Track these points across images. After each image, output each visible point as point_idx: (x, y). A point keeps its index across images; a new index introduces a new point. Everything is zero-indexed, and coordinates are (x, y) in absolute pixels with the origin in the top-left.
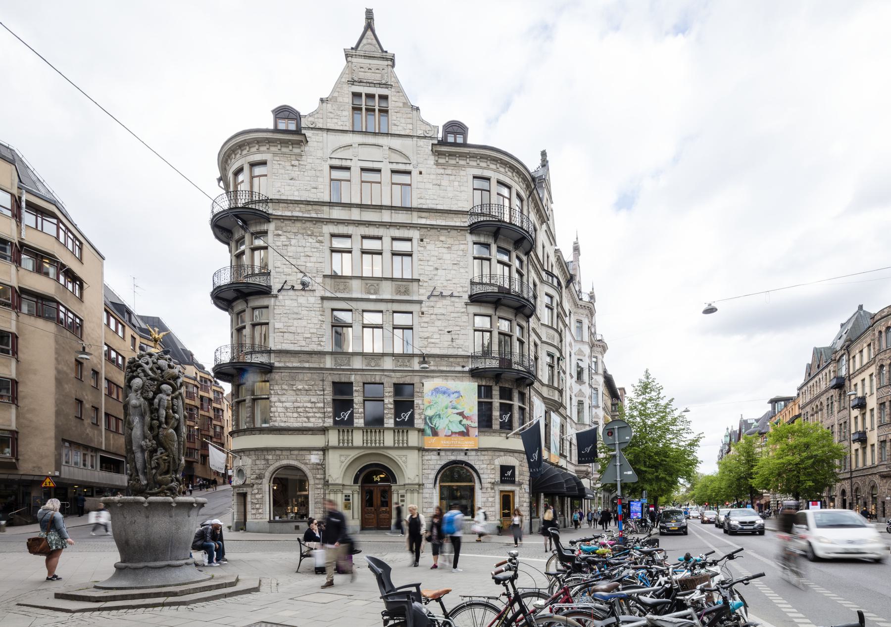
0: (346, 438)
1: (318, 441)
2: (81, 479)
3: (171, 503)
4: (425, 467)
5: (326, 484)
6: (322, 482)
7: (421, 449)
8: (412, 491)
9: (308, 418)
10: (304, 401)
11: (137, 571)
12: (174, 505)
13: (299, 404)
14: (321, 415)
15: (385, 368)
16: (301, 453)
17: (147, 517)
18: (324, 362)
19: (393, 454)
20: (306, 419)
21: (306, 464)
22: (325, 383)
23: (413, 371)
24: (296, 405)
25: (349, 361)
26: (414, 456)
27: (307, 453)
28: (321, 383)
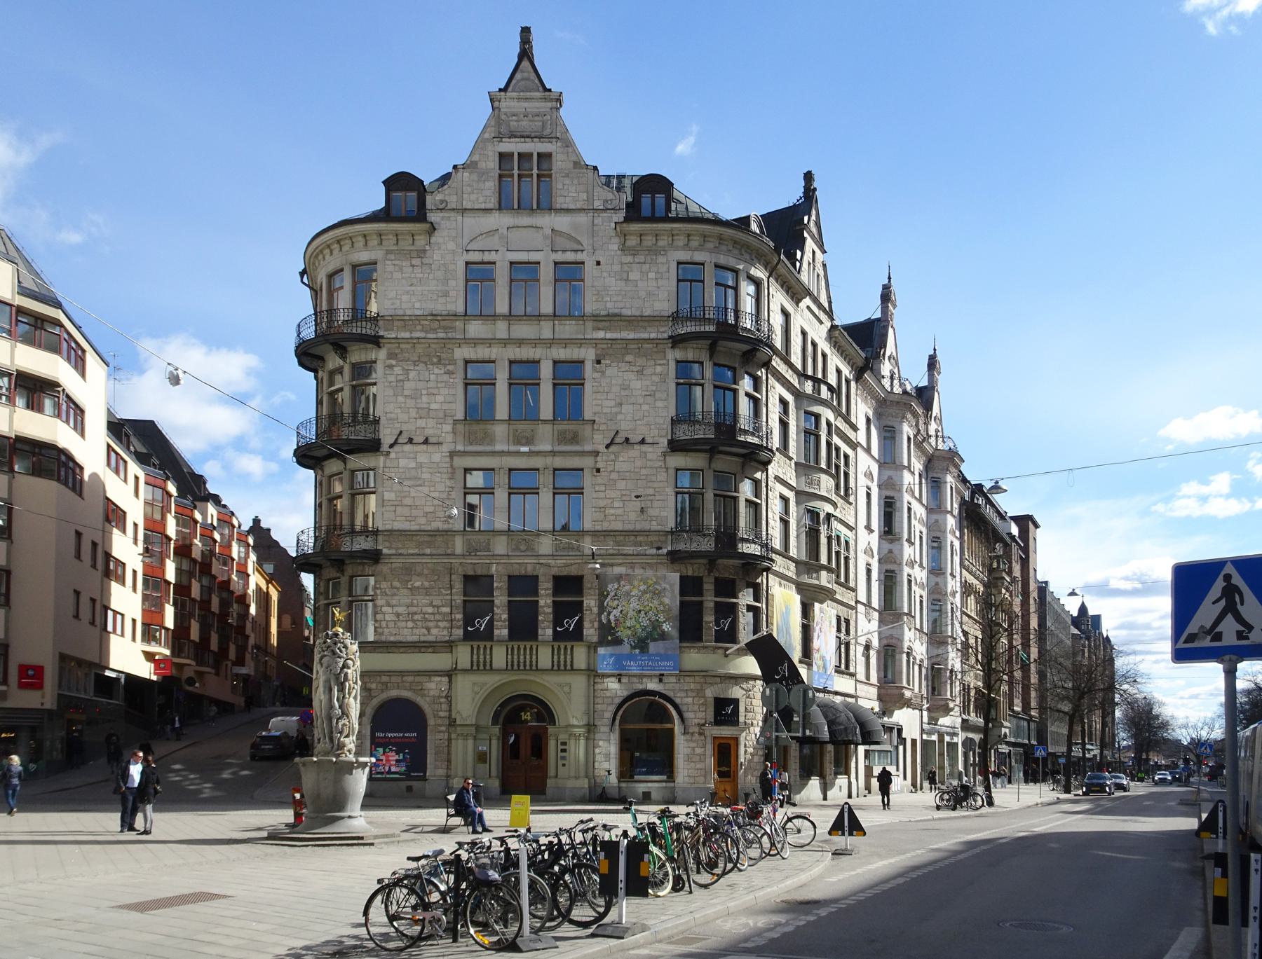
1: (441, 661)
9: (428, 629)
13: (415, 609)
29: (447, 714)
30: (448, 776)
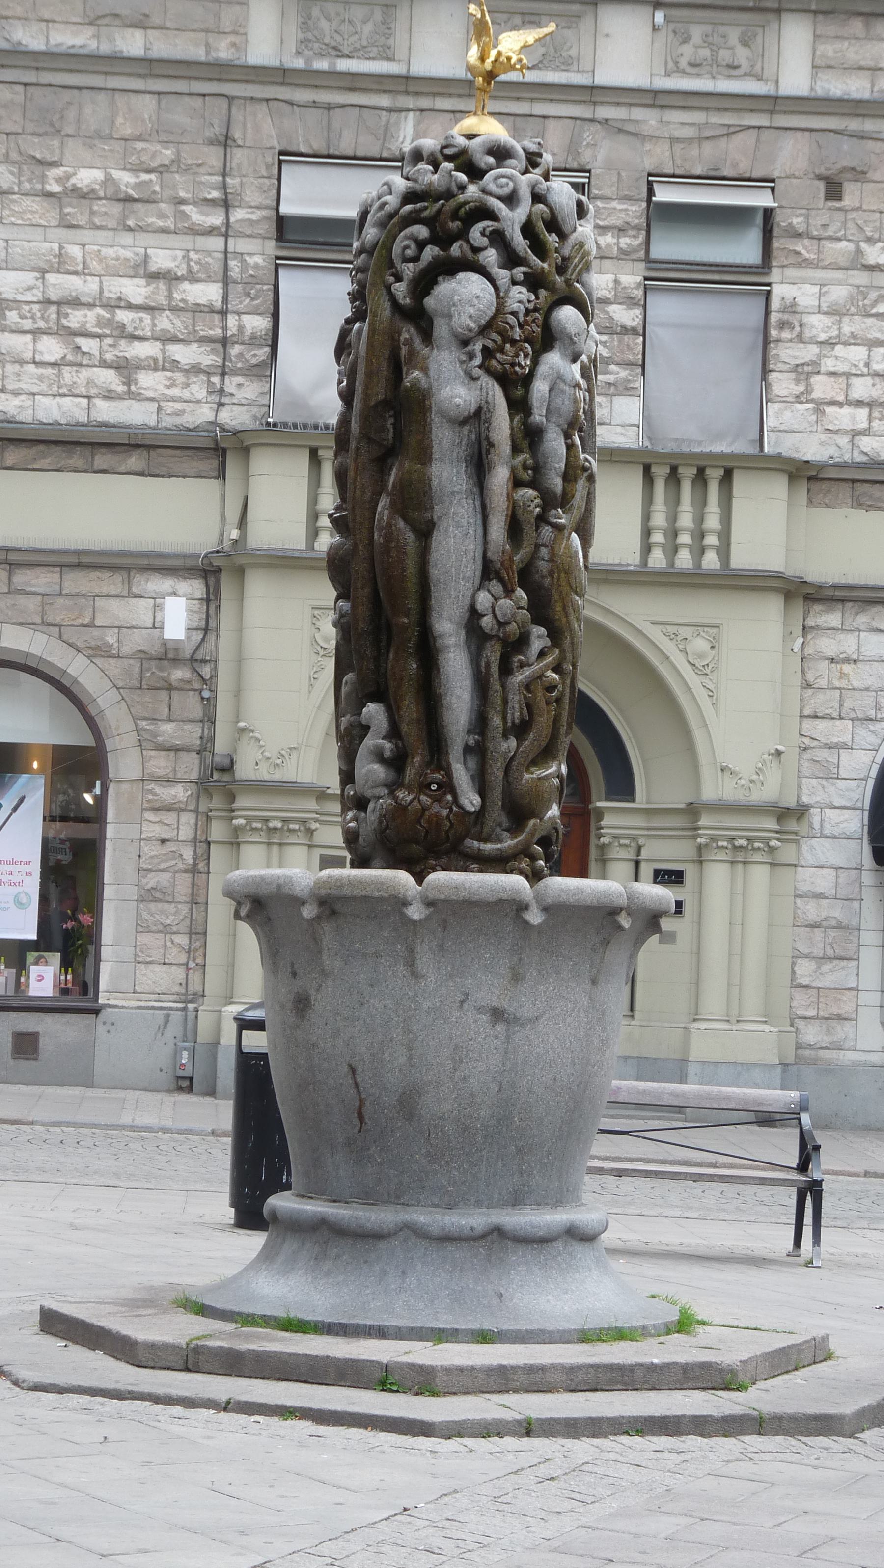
0: (686, 520)
1: (175, 513)
2: (454, 776)
3: (522, 907)
4: (819, 702)
5: (219, 780)
6: (190, 766)
7: (803, 595)
8: (740, 854)
9: (126, 368)
10: (107, 264)
11: (450, 1247)
12: (415, 912)
13: (74, 284)
14: (206, 358)
15: (602, 78)
16: (76, 582)
17: (516, 978)
18: (239, 31)
19: (636, 616)
20: (109, 378)
21: (98, 652)
22: (238, 156)
23: (774, 103)
24: (61, 284)
25: (387, 28)
26: (757, 632)
27: (111, 583)
28: (213, 157)
29: (192, 734)
30: (191, 998)
